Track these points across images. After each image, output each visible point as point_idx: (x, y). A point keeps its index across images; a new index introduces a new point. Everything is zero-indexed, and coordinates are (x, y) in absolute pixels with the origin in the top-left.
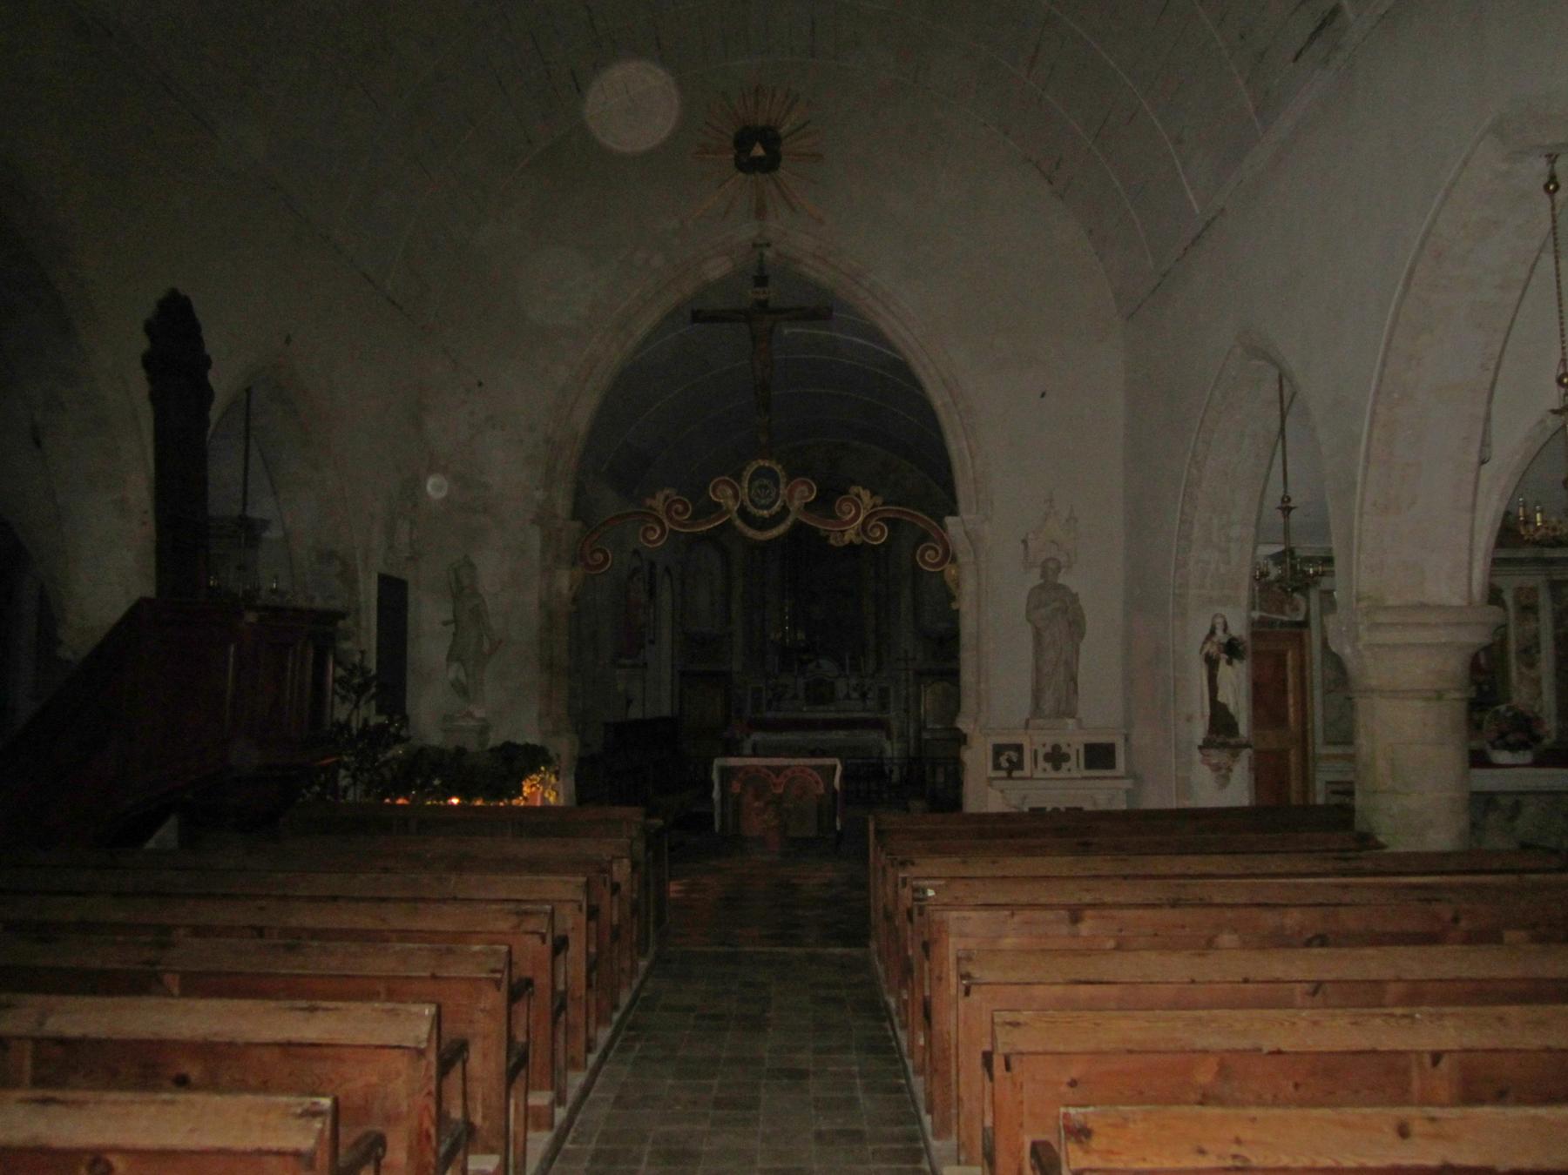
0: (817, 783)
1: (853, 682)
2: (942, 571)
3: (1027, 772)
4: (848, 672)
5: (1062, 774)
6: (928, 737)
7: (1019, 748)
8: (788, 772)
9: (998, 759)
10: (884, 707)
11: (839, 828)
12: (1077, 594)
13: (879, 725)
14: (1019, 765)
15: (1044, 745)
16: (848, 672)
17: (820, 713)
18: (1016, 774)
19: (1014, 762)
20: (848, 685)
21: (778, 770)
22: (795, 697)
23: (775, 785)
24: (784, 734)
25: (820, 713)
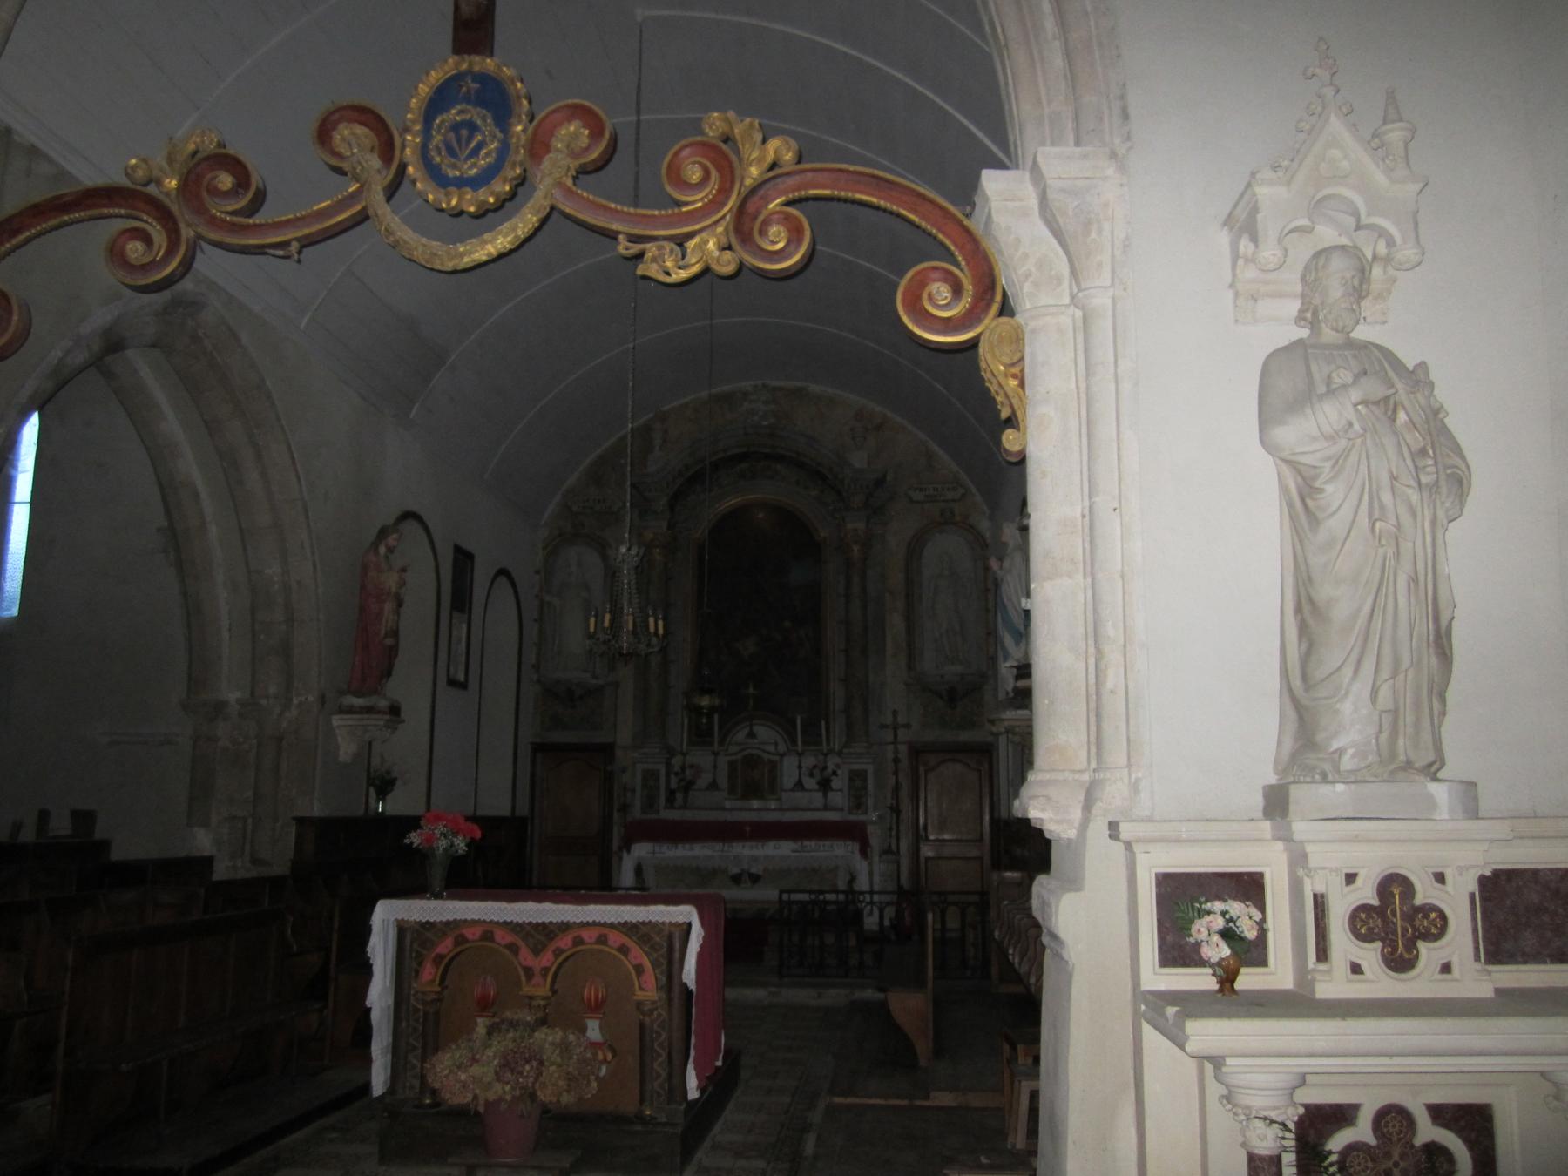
0: (639, 970)
1: (809, 761)
2: (973, 345)
3: (1278, 973)
4: (800, 748)
5: (1421, 983)
6: (930, 854)
7: (1249, 887)
8: (565, 942)
9: (1185, 929)
10: (858, 803)
11: (693, 1093)
12: (1422, 365)
13: (853, 832)
14: (1251, 951)
15: (1351, 878)
16: (800, 748)
17: (756, 810)
18: (1248, 980)
19: (1242, 939)
20: (800, 767)
21: (543, 934)
22: (713, 786)
23: (529, 972)
24: (680, 846)
25: (756, 810)
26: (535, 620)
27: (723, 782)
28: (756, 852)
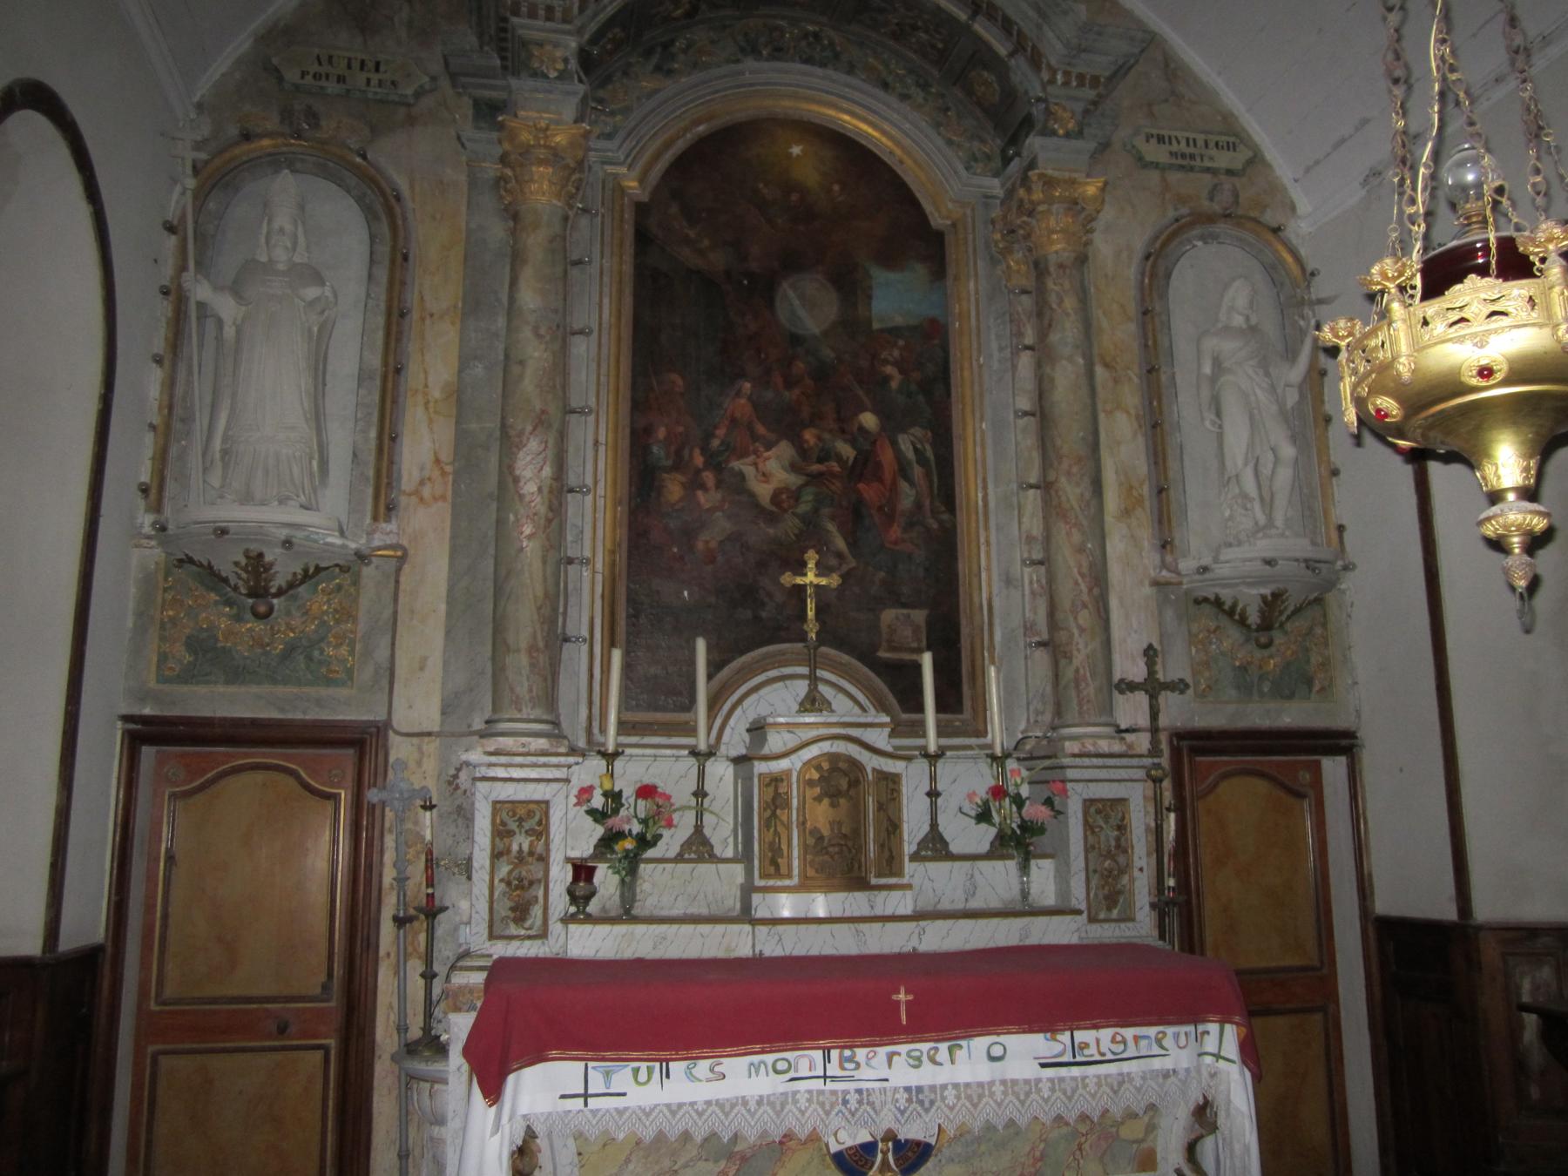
16: (932, 742)
24: (677, 1067)
26: (158, 360)
27: (722, 834)
28: (926, 1076)
